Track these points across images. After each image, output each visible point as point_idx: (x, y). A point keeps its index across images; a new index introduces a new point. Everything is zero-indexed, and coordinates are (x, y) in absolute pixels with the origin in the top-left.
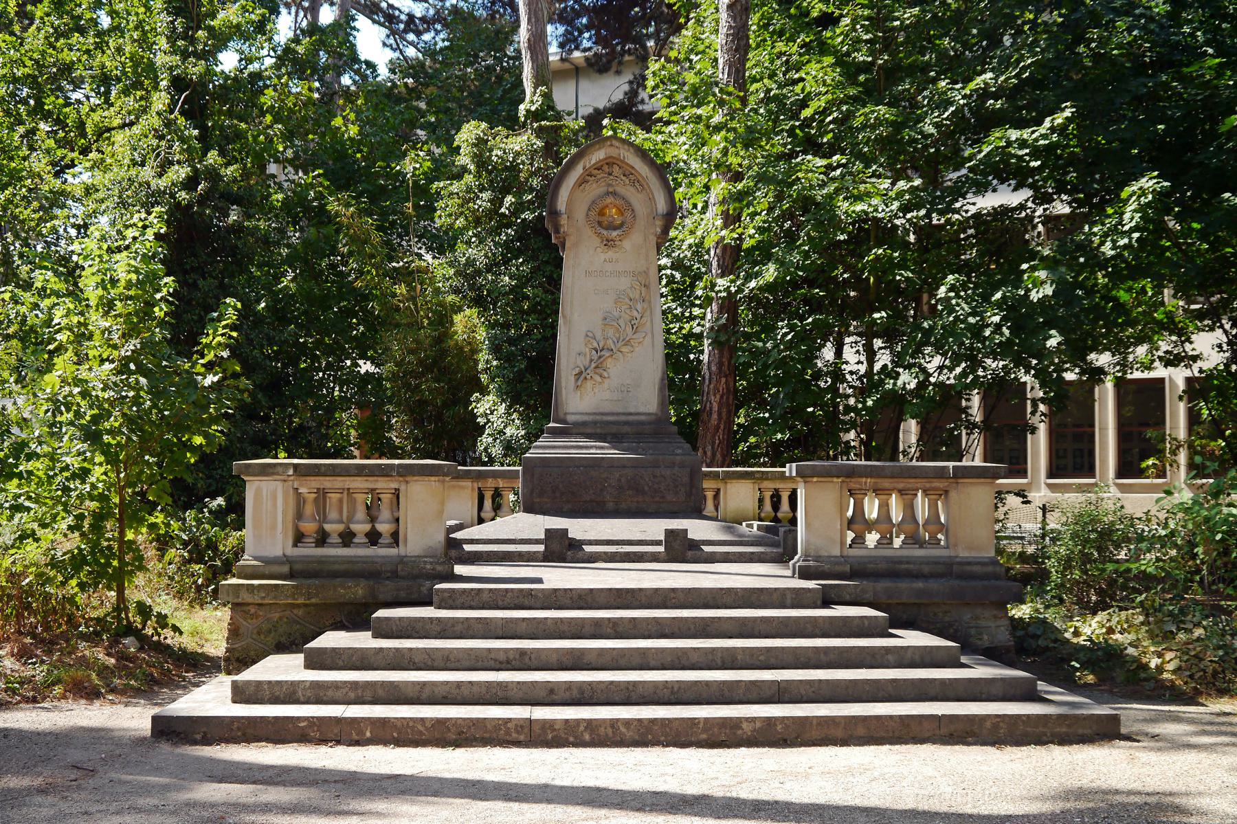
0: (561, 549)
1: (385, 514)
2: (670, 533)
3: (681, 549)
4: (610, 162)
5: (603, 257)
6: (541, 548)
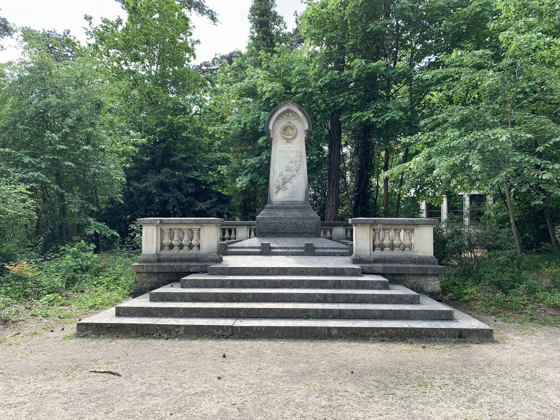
0: (266, 251)
1: (195, 238)
2: (307, 245)
3: (310, 251)
4: (288, 111)
5: (286, 145)
6: (259, 250)
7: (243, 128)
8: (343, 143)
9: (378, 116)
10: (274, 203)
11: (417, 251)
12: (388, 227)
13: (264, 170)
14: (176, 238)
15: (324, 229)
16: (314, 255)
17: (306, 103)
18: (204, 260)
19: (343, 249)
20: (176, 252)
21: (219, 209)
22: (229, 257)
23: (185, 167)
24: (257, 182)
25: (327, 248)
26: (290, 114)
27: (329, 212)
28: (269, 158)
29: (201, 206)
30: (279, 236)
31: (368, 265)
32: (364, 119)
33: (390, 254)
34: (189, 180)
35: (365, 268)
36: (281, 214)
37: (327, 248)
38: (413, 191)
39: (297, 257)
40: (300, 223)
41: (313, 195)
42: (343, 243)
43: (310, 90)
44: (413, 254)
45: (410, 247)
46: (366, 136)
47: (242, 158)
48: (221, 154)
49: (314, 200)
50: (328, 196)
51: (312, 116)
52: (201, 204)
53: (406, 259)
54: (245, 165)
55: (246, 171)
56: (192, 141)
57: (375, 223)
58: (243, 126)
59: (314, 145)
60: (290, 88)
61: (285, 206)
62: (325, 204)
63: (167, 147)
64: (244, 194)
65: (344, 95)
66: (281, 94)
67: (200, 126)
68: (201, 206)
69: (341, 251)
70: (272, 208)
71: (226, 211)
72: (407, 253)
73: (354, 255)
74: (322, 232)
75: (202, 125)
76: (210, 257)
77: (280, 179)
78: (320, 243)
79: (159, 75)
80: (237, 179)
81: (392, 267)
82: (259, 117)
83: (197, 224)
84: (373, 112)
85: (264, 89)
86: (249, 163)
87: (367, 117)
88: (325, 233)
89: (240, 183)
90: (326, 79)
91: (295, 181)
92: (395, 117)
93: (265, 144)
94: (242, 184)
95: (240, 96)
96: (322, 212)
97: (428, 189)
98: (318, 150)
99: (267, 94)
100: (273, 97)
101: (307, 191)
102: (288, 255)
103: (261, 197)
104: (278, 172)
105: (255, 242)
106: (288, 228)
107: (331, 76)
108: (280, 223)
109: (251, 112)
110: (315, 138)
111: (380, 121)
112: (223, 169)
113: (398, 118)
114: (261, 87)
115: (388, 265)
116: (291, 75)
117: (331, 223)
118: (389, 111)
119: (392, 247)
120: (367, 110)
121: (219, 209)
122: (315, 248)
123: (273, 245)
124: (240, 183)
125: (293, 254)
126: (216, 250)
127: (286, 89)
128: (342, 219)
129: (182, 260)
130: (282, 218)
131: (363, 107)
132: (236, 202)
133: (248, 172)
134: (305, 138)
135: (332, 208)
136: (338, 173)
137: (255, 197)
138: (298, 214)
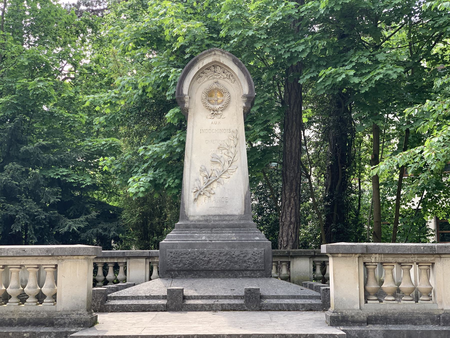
1: (48, 282)
2: (249, 292)
5: (211, 121)
6: (164, 302)
7: (141, 96)
8: (305, 120)
9: (362, 75)
10: (191, 219)
11: (441, 302)
12: (390, 259)
13: (175, 164)
14: (13, 282)
15: (277, 262)
16: (261, 309)
17: (243, 52)
18: (62, 322)
19: (311, 297)
20: (12, 308)
21: (100, 231)
22: (110, 314)
23: (45, 162)
24: (163, 185)
25: (283, 297)
27: (285, 234)
28: (182, 144)
29: (71, 225)
30: (200, 277)
31: (357, 328)
32: (340, 79)
33: (394, 307)
34: (52, 182)
35: (353, 334)
36: (204, 237)
37: (283, 297)
38: (417, 199)
39: (232, 313)
40: (237, 254)
41: (257, 205)
42: (311, 287)
43: (251, 33)
44: (435, 307)
45: (429, 293)
46: (340, 106)
47: (139, 144)
48: (107, 139)
49: (259, 214)
50: (283, 206)
51: (255, 77)
52: (70, 222)
53: (422, 317)
54: (144, 155)
55: (146, 165)
56: (58, 118)
57: (367, 252)
58: (140, 92)
59: (258, 122)
60: (218, 32)
61: (208, 224)
62: (277, 221)
63: (16, 128)
64: (142, 205)
65: (306, 42)
66: (202, 40)
67: (72, 95)
68: (71, 225)
69: (308, 301)
70: (187, 227)
71: (112, 234)
72: (423, 305)
73: (332, 309)
74: (274, 268)
75: (77, 93)
76: (75, 316)
77: (201, 178)
78: (272, 287)
79: (9, 16)
80: (130, 180)
81: (400, 332)
82: (167, 76)
83: (52, 256)
84: (353, 68)
85: (176, 31)
86: (150, 152)
87: (343, 76)
88: (278, 269)
89: (135, 185)
90: (275, 16)
91: (226, 181)
92: (390, 75)
93: (176, 120)
94: (139, 188)
95: (137, 43)
96: (272, 232)
97: (440, 197)
98: (265, 129)
99: (180, 39)
100: (190, 44)
101: (247, 200)
102: (215, 311)
103: (171, 208)
104: (197, 165)
105: (158, 287)
106: (214, 261)
107: (283, 10)
108: (202, 253)
109: (155, 70)
110: (260, 110)
111: (363, 83)
112: (105, 162)
113: (395, 76)
114: (170, 29)
115: (392, 328)
116: (218, 11)
117: (289, 252)
118: (380, 66)
119: (397, 293)
120: (343, 66)
121: (100, 231)
122: (262, 297)
123: (188, 292)
124: (135, 185)
125: (224, 308)
126: (85, 305)
127: (212, 33)
128: (305, 245)
129: (23, 323)
130: (204, 245)
131: (337, 61)
132: (130, 218)
133: (148, 168)
134: (244, 108)
135: (289, 226)
136: (299, 169)
137: (161, 209)
138: (232, 236)
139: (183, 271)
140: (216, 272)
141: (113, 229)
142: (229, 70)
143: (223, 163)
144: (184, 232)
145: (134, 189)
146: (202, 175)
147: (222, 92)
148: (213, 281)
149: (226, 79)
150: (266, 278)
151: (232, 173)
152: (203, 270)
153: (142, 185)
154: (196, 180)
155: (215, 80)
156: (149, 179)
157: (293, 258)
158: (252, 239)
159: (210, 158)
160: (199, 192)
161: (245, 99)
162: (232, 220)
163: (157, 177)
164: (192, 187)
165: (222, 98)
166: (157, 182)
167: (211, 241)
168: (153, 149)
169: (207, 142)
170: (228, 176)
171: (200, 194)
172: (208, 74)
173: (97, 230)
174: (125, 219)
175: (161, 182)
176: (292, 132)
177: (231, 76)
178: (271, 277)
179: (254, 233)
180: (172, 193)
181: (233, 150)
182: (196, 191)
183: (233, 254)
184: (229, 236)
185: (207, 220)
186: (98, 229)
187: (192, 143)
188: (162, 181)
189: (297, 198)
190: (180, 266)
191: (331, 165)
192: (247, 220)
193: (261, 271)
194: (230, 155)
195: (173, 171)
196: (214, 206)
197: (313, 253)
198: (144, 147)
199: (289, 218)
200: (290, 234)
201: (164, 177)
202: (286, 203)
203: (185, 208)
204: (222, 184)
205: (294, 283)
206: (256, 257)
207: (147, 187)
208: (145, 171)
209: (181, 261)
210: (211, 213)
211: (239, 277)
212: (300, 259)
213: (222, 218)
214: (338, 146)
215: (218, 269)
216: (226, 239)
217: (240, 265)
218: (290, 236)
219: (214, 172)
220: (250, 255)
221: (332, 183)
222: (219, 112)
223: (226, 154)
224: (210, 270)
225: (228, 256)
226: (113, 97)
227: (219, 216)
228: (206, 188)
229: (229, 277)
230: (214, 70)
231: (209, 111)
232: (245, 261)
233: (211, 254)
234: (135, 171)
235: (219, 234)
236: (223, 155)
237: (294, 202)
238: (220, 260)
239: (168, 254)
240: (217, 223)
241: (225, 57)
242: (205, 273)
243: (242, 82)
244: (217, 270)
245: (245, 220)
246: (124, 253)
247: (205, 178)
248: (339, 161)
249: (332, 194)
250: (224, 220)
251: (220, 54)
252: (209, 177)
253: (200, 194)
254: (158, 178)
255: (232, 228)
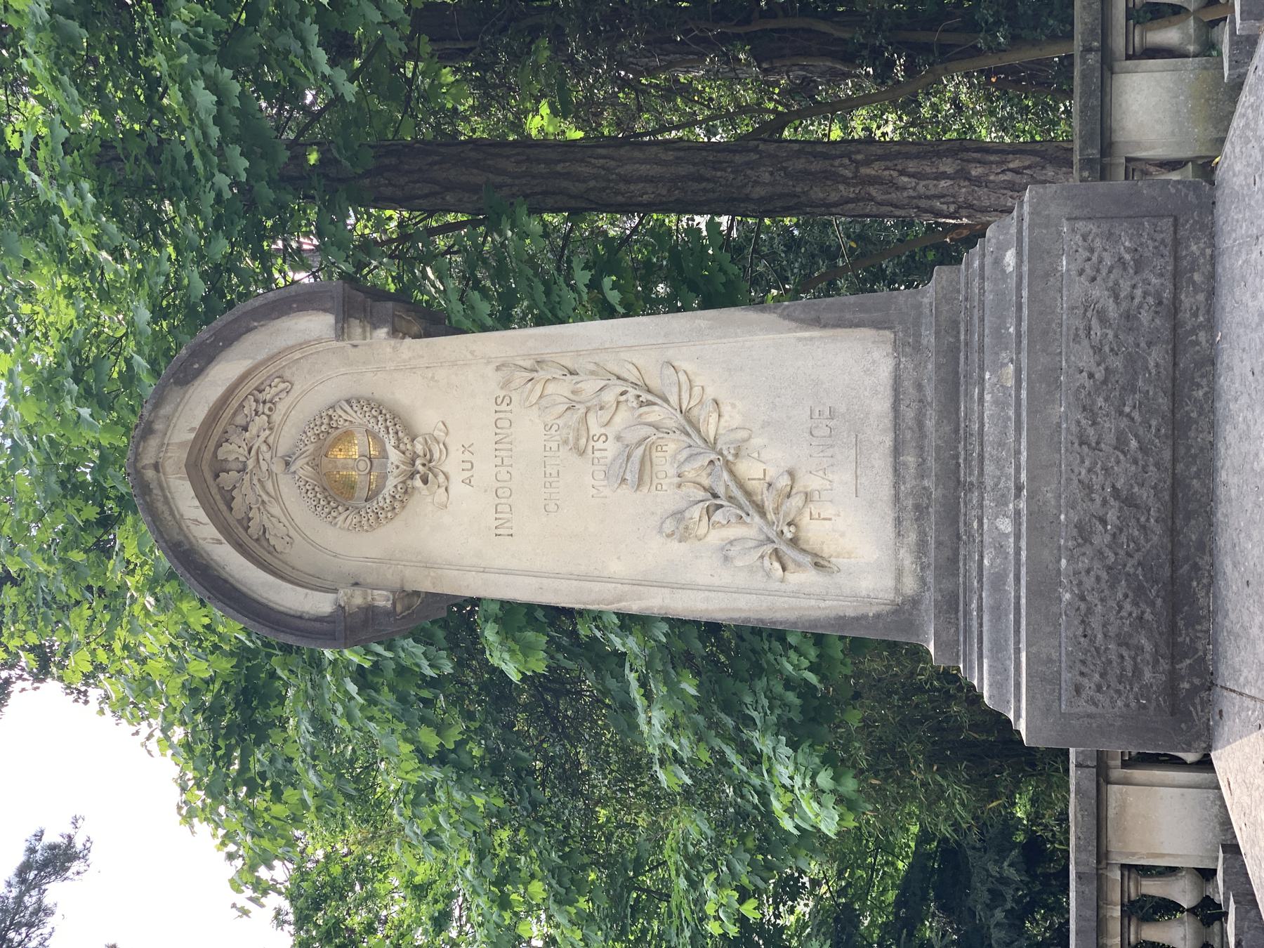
4: (208, 468)
5: (457, 487)
10: (910, 585)
13: (723, 657)
21: (999, 915)
24: (806, 690)
26: (233, 451)
30: (1206, 545)
40: (1086, 359)
55: (732, 756)
61: (939, 503)
64: (903, 761)
70: (951, 605)
80: (787, 824)
91: (732, 417)
104: (659, 553)
106: (1123, 473)
108: (1083, 533)
124: (810, 808)
130: (1038, 524)
134: (397, 332)
135: (977, 182)
138: (1000, 383)
139: (1173, 629)
140: (1180, 467)
141: (993, 869)
142: (235, 404)
143: (651, 430)
144: (975, 624)
145: (823, 813)
146: (703, 529)
147: (328, 433)
148: (1234, 480)
149: (276, 418)
150: (1219, 209)
151: (697, 390)
152: (1173, 532)
153: (808, 782)
154: (726, 558)
155: (278, 467)
156: (785, 751)
157: (1111, 144)
158: (1013, 282)
159: (625, 490)
160: (783, 548)
161: (356, 327)
162: (919, 387)
163: (774, 718)
164: (759, 581)
165: (360, 438)
166: (796, 717)
167: (1019, 489)
168: (657, 734)
169: (552, 507)
170: (711, 407)
171: (794, 542)
172: (251, 498)
173: (998, 925)
174: (956, 826)
175: (798, 701)
176: (596, 178)
177: (261, 397)
178: (1207, 168)
179: (982, 278)
180: (841, 656)
181: (590, 386)
182: (780, 560)
183: (1091, 376)
184: (996, 402)
185: (917, 507)
186: (993, 922)
187: (557, 576)
188: (791, 697)
189: (859, 152)
190: (1148, 647)
191: (751, 53)
192: (920, 314)
193: (1181, 233)
194: (609, 397)
195: (753, 651)
196: (848, 477)
197: (1093, 58)
198: (656, 767)
199: (943, 184)
200: (1009, 176)
201: (779, 688)
202: (880, 197)
203: (861, 611)
204: (744, 434)
205: (1222, 141)
206: (1108, 261)
207: (817, 760)
208: (755, 760)
209: (1123, 642)
210: (886, 492)
211: (1213, 344)
212: (1116, 114)
213: (909, 435)
214: (685, 33)
215: (1167, 455)
216: (1011, 413)
217: (1149, 344)
218: (1017, 178)
219: (690, 475)
220: (1096, 293)
221: (824, 54)
222: (419, 448)
223: (605, 415)
224: (1173, 496)
225: (1100, 402)
226: (479, 875)
227: (897, 451)
228: (763, 514)
229: (1212, 395)
230: (233, 474)
231: (416, 496)
232: (1127, 316)
233: (1088, 488)
234: (756, 801)
235: (988, 449)
236: (611, 431)
237: (876, 165)
238: (1121, 445)
239: (1082, 706)
240: (931, 462)
241: (169, 418)
242: (1188, 518)
243: (281, 342)
244: (1174, 461)
245: (917, 324)
246: (1079, 876)
247: (718, 516)
248: (741, 30)
249: (865, 53)
250: (920, 424)
251: (153, 442)
252: (715, 496)
253: (794, 542)
254: (778, 711)
255: (956, 385)
